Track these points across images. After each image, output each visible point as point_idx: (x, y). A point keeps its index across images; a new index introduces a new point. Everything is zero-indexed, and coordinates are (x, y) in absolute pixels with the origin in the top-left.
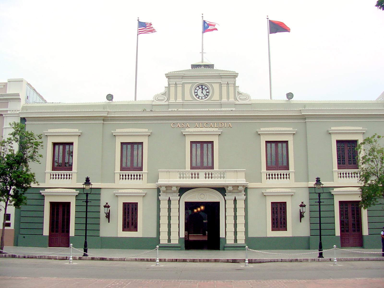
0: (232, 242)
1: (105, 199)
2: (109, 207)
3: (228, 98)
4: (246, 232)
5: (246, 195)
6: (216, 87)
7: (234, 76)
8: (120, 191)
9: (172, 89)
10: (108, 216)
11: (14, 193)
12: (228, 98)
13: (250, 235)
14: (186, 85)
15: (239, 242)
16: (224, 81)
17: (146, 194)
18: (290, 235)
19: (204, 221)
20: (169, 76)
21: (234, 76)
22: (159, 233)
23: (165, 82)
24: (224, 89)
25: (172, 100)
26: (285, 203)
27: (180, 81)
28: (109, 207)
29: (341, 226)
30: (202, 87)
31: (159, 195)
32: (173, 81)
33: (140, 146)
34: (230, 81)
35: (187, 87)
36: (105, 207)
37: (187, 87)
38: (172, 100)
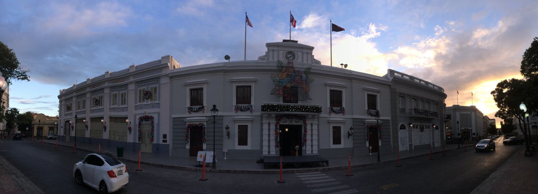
0: (310, 152)
1: (226, 123)
2: (229, 128)
3: (307, 61)
4: (318, 146)
5: (318, 121)
6: (300, 54)
7: (312, 48)
8: (236, 117)
9: (271, 53)
10: (228, 135)
11: (368, 26)
12: (307, 61)
13: (320, 148)
14: (280, 52)
15: (314, 152)
16: (305, 51)
17: (253, 119)
18: (343, 147)
19: (401, 148)
20: (268, 45)
21: (312, 48)
22: (262, 146)
23: (266, 49)
24: (305, 56)
25: (271, 60)
26: (247, 126)
27: (275, 48)
28: (229, 128)
29: (35, 117)
30: (290, 53)
31: (262, 120)
32: (271, 48)
33: (249, 88)
34: (309, 51)
35: (281, 53)
36: (226, 128)
37: (281, 53)
38: (271, 60)
